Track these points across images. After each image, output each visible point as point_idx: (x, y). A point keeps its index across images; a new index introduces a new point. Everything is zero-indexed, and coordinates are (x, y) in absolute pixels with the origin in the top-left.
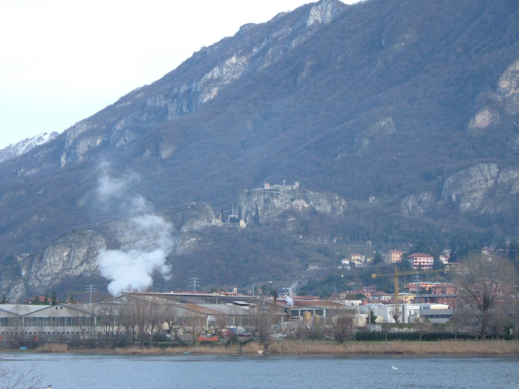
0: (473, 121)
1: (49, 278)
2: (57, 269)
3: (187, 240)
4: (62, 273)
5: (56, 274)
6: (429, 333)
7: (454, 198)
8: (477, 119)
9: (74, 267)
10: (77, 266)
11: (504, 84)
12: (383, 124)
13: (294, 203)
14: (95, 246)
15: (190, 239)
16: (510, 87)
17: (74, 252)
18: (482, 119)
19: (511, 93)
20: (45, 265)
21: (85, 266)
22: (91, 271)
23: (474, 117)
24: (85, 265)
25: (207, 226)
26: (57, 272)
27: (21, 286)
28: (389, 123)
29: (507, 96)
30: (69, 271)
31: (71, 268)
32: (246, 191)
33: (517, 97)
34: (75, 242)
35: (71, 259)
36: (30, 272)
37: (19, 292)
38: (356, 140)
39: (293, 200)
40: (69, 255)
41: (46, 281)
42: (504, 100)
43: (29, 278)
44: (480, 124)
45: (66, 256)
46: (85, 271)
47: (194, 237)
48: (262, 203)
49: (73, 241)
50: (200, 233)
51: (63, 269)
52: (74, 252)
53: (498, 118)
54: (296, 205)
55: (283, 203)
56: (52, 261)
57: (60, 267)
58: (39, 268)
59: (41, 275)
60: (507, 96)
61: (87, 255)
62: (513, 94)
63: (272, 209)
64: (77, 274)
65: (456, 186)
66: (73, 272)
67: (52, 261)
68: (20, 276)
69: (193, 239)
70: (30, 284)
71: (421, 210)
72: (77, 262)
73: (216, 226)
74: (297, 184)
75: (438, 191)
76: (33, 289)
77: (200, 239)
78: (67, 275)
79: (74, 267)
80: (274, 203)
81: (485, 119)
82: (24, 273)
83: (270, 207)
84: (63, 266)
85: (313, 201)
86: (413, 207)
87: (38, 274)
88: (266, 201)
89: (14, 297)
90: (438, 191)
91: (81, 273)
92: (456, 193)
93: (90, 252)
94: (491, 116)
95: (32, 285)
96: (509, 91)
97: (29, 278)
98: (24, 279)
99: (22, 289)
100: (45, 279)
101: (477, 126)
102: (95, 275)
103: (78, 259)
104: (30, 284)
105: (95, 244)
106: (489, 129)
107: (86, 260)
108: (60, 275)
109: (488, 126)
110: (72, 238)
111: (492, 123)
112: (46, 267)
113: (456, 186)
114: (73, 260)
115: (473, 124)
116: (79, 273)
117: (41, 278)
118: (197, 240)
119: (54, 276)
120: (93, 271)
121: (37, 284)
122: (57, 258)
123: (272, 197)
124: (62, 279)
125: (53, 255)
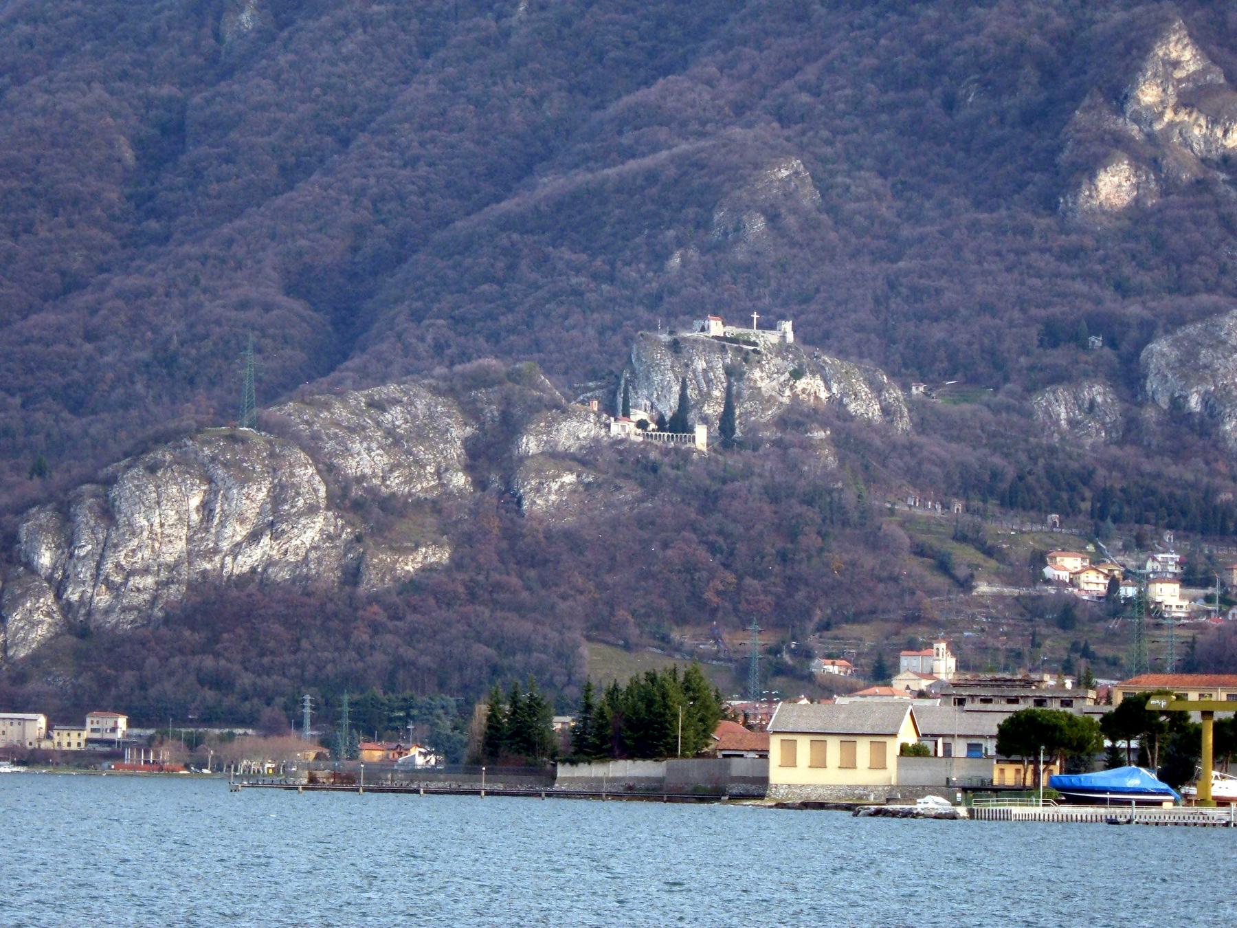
0: (1090, 190)
1: (150, 581)
2: (175, 549)
3: (554, 478)
4: (190, 563)
5: (171, 568)
6: (770, 807)
7: (1194, 403)
8: (1101, 185)
9: (225, 545)
10: (238, 545)
11: (1149, 94)
12: (784, 173)
13: (801, 384)
14: (295, 480)
15: (559, 476)
16: (1162, 102)
17: (225, 497)
18: (1114, 185)
19: (1166, 120)
20: (133, 533)
21: (266, 546)
22: (289, 563)
23: (1093, 176)
24: (266, 540)
25: (596, 440)
26: (170, 559)
27: (48, 600)
28: (796, 173)
29: (1158, 127)
30: (211, 560)
31: (216, 551)
32: (665, 337)
33: (1181, 133)
34: (226, 465)
35: (216, 521)
36: (71, 556)
37: (41, 622)
38: (718, 216)
39: (797, 375)
40: (206, 508)
41: (138, 590)
42: (1151, 137)
43: (66, 577)
44: (1107, 199)
45: (197, 509)
46: (270, 563)
47: (571, 471)
48: (723, 378)
49: (213, 459)
50: (584, 459)
51: (189, 553)
52: (225, 497)
53: (1153, 185)
54: (804, 391)
55: (775, 383)
56: (157, 521)
57: (180, 546)
58: (105, 549)
59: (118, 566)
60: (1158, 127)
61: (275, 511)
62: (1171, 124)
63: (751, 398)
64: (236, 571)
65: (1190, 368)
66: (223, 566)
67: (157, 521)
68: (31, 568)
69: (569, 478)
70: (75, 598)
71: (1098, 432)
72: (238, 532)
73: (622, 441)
74: (787, 326)
75: (1129, 378)
76: (89, 614)
77: (591, 479)
78: (204, 573)
79: (225, 545)
80: (755, 381)
81: (1120, 185)
82: (45, 559)
83: (746, 393)
84: (189, 540)
85: (840, 383)
86: (1073, 423)
87: (109, 566)
88: (729, 372)
89: (24, 639)
90: (1129, 378)
91: (253, 570)
92: (1202, 388)
93: (285, 501)
94: (1134, 180)
95: (81, 601)
96: (1161, 114)
97: (66, 577)
98: (49, 579)
99: (49, 614)
100: (135, 581)
101: (1101, 204)
102: (307, 577)
103: (242, 521)
104: (75, 598)
105: (292, 475)
106: (1136, 213)
107: (272, 524)
108: (184, 569)
109: (1128, 208)
110: (207, 451)
111: (1137, 200)
112: (135, 542)
113: (1190, 368)
114: (222, 524)
115: (1091, 196)
116: (246, 569)
117: (118, 579)
118: (580, 482)
119: (164, 575)
120: (297, 565)
121: (103, 599)
122: (172, 517)
123: (746, 360)
124: (191, 585)
125: (158, 503)
